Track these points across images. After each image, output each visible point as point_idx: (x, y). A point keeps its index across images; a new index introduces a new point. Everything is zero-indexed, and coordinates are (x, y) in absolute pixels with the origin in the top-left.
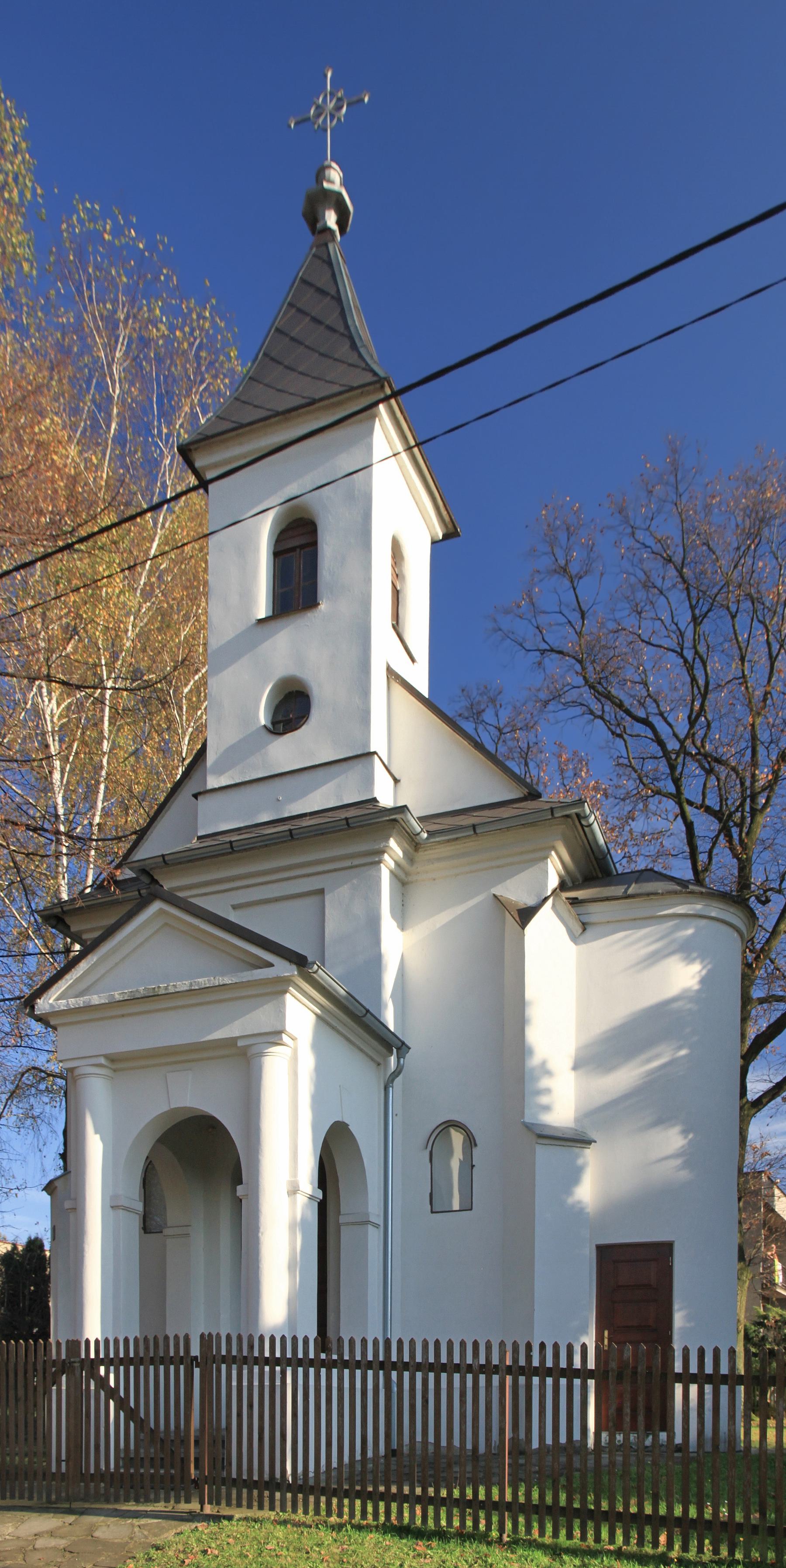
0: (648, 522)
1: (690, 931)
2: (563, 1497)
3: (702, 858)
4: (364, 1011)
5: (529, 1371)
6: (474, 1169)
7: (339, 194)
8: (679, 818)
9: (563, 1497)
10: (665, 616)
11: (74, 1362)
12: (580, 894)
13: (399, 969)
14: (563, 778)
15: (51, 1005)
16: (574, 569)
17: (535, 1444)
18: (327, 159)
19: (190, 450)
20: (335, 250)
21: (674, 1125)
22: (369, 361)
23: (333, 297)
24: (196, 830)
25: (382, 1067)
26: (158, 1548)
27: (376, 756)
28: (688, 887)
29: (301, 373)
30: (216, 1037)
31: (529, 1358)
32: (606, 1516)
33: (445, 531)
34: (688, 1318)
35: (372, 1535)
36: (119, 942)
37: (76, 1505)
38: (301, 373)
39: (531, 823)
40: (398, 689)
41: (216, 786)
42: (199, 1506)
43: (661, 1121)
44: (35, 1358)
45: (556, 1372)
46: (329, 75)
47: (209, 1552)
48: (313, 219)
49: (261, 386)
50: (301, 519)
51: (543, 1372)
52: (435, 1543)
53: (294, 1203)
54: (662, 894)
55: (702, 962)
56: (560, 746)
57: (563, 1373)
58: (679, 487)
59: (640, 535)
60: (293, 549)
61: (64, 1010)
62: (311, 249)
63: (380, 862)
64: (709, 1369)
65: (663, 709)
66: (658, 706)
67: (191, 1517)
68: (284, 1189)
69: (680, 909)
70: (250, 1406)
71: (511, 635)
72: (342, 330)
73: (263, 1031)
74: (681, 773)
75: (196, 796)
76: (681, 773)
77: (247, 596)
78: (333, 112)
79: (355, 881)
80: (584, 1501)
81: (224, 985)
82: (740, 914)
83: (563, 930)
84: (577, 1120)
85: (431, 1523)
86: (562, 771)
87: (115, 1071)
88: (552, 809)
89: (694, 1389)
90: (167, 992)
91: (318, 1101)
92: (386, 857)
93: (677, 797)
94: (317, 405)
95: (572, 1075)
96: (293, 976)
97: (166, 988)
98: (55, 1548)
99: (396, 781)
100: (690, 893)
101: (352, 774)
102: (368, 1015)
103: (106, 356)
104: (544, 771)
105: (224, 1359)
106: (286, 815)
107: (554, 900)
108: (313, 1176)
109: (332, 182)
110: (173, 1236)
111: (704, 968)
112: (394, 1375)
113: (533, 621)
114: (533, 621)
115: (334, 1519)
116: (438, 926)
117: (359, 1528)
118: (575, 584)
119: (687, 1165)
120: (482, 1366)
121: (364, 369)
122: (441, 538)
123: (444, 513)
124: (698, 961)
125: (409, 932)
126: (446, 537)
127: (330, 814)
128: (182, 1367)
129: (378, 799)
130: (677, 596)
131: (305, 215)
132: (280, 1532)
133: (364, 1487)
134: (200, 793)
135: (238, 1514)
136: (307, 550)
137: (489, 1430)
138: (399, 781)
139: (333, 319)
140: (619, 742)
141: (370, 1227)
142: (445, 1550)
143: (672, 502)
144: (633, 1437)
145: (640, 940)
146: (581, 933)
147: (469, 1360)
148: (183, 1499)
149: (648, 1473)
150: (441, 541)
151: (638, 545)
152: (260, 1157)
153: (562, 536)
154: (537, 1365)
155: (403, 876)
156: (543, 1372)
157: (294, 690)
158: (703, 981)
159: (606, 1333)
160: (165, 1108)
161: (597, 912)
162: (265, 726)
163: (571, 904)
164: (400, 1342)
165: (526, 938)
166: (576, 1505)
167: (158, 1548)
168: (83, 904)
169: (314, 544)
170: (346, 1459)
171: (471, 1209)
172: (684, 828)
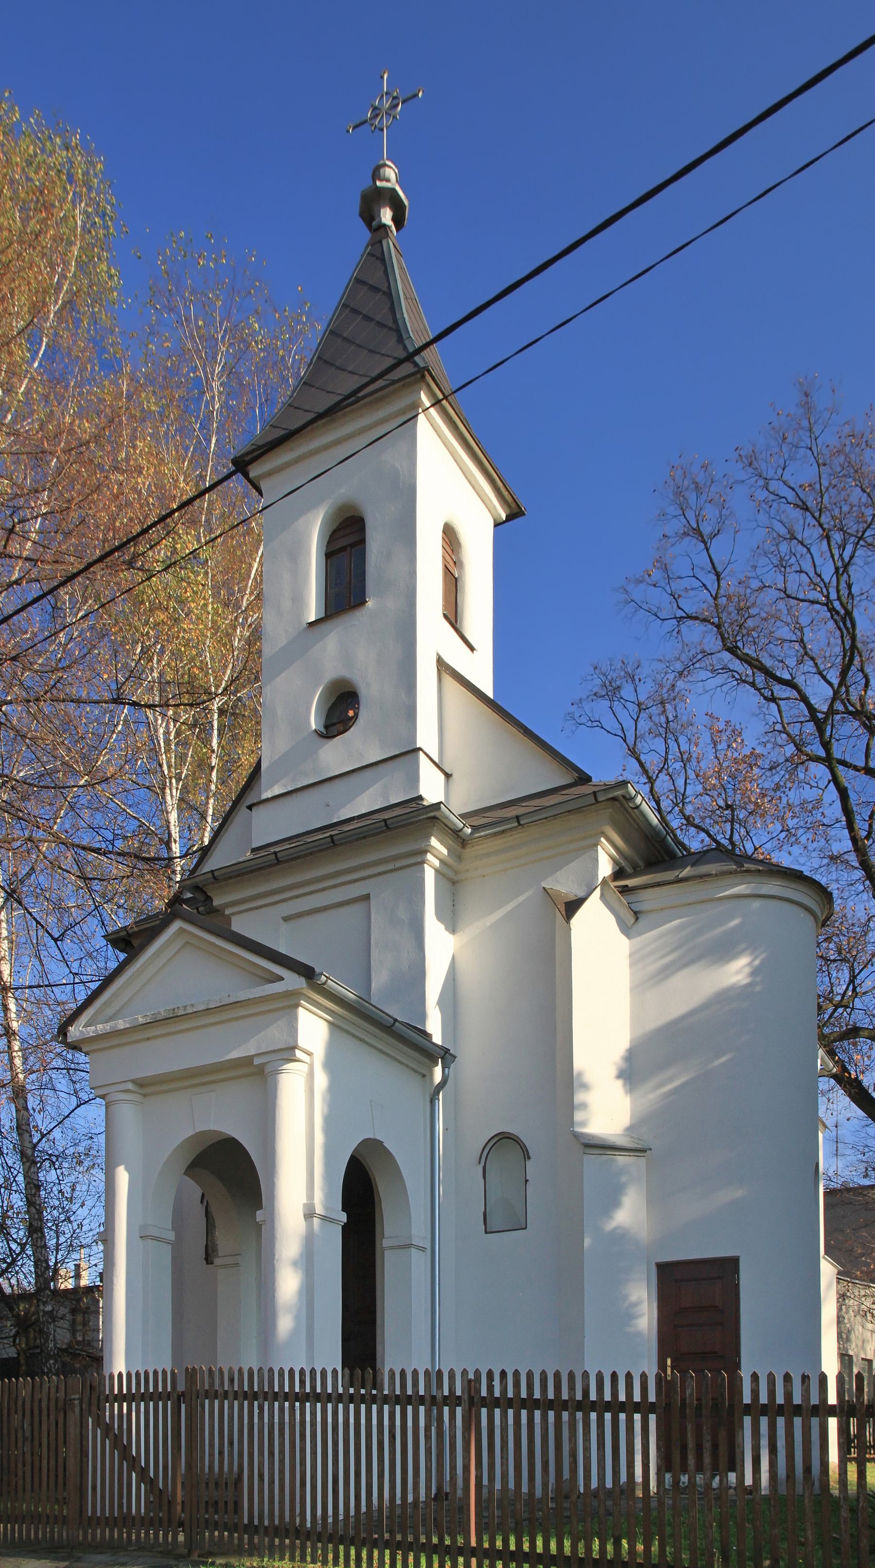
4: (392, 1021)
7: (394, 190)
10: (807, 566)
11: (74, 1399)
12: (630, 882)
16: (706, 530)
20: (390, 245)
23: (384, 293)
27: (421, 752)
33: (508, 512)
36: (143, 964)
40: (449, 681)
48: (369, 216)
50: (353, 517)
57: (523, 1404)
58: (814, 430)
59: (774, 486)
61: (93, 1036)
63: (423, 862)
64: (764, 1399)
70: (231, 1443)
71: (645, 606)
77: (298, 600)
82: (811, 893)
83: (611, 919)
86: (715, 744)
87: (145, 1096)
88: (595, 793)
92: (429, 856)
93: (829, 761)
94: (362, 402)
99: (448, 776)
102: (397, 1023)
105: (207, 1395)
107: (602, 890)
109: (388, 180)
110: (225, 1266)
113: (668, 588)
114: (668, 588)
116: (488, 924)
118: (708, 545)
122: (504, 519)
123: (506, 493)
126: (510, 518)
127: (375, 816)
128: (169, 1403)
129: (424, 796)
131: (362, 215)
138: (451, 775)
140: (773, 706)
143: (807, 448)
144: (699, 1479)
150: (504, 522)
151: (772, 497)
152: (276, 1180)
153: (692, 497)
160: (190, 1133)
161: (649, 899)
162: (315, 730)
163: (620, 892)
169: (362, 541)
171: (526, 1228)
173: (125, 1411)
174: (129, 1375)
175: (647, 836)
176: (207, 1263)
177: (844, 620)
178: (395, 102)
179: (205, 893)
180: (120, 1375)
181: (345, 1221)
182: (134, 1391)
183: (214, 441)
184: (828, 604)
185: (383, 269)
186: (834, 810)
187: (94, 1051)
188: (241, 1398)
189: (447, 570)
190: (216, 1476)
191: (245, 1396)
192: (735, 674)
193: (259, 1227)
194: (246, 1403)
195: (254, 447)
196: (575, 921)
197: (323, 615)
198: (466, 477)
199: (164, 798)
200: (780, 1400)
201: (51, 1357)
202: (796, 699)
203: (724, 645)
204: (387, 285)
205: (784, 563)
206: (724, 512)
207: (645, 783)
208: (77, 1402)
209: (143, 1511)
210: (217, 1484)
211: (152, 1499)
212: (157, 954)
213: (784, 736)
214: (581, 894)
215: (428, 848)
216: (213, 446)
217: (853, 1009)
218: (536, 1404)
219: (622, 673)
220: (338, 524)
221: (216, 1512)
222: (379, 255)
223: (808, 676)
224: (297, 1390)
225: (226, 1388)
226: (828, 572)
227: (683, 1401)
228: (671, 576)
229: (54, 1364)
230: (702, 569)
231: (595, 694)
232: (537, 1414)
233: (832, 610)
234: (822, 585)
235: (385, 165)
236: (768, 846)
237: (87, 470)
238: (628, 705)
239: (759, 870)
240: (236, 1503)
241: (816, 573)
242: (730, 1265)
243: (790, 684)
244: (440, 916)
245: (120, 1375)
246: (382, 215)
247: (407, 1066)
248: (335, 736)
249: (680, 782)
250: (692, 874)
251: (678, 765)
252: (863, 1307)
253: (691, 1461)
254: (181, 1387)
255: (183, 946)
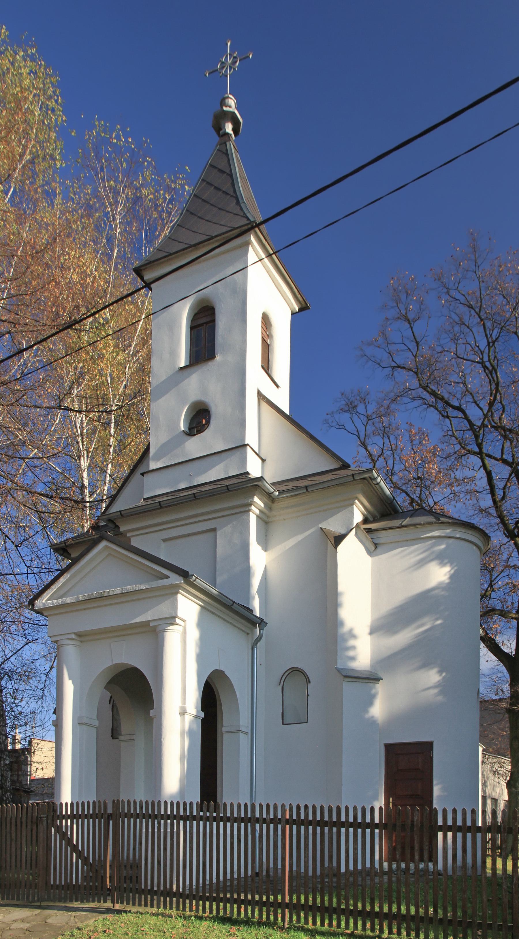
0: (456, 285)
1: (443, 547)
2: (431, 910)
3: (499, 494)
4: (232, 603)
5: (339, 824)
6: (309, 697)
7: (234, 113)
8: (482, 468)
9: (431, 910)
11: (43, 817)
13: (263, 575)
14: (412, 445)
15: (44, 604)
16: (411, 316)
17: (343, 870)
18: (227, 93)
19: (141, 270)
20: (231, 146)
21: (433, 668)
22: (246, 212)
23: (228, 174)
24: (142, 494)
25: (250, 635)
26: (79, 929)
28: (439, 520)
29: (207, 221)
30: (138, 621)
31: (298, 814)
32: (343, 911)
33: (300, 307)
34: (444, 789)
35: (206, 922)
37: (44, 904)
38: (207, 221)
39: (342, 484)
40: (264, 405)
41: (155, 468)
42: (112, 904)
43: (426, 665)
44: (22, 814)
45: (355, 825)
46: (229, 44)
47: (107, 932)
48: (218, 128)
49: (184, 229)
50: (207, 306)
51: (348, 825)
52: (242, 928)
53: (183, 720)
54: (424, 524)
55: (451, 565)
56: (410, 425)
57: (318, 823)
58: (478, 261)
60: (201, 325)
62: (217, 146)
63: (249, 511)
64: (459, 823)
65: (476, 399)
66: (473, 397)
67: (108, 911)
68: (177, 712)
69: (436, 533)
70: (141, 843)
71: (373, 359)
72: (232, 193)
73: (164, 617)
74: (482, 440)
75: (143, 474)
76: (482, 440)
77: (174, 354)
78: (231, 65)
79: (234, 523)
80: (347, 905)
81: (141, 590)
83: (363, 548)
84: (372, 666)
85: (242, 915)
86: (412, 441)
87: (82, 642)
88: (353, 475)
89: (450, 834)
90: (109, 594)
91: (201, 658)
92: (253, 507)
93: (480, 454)
95: (369, 638)
96: (181, 583)
97: (108, 592)
98: (22, 929)
99: (263, 460)
100: (441, 523)
101: (235, 457)
103: (112, 210)
104: (400, 441)
105: (126, 815)
106: (195, 484)
107: (356, 530)
108: (197, 703)
109: (230, 107)
111: (452, 569)
112: (257, 825)
113: (387, 349)
114: (387, 349)
115: (188, 913)
116: (287, 548)
117: (200, 918)
118: (412, 325)
119: (441, 693)
120: (272, 819)
121: (242, 216)
123: (299, 296)
124: (448, 565)
125: (269, 552)
126: (301, 310)
127: (220, 483)
128: (102, 820)
129: (250, 472)
130: (478, 330)
132: (153, 920)
133: (218, 895)
134: (145, 473)
135: (134, 909)
136: (209, 325)
137: (275, 859)
139: (226, 187)
140: (447, 420)
141: (241, 735)
142: (247, 931)
143: (473, 271)
145: (411, 553)
146: (374, 550)
147: (264, 816)
148: (102, 901)
149: (394, 886)
150: (297, 312)
152: (163, 693)
153: (403, 297)
154: (303, 818)
155: (265, 518)
156: (348, 825)
157: (202, 408)
158: (452, 577)
159: (391, 800)
160: (111, 664)
161: (384, 537)
162: (183, 431)
163: (367, 532)
164: (261, 806)
165: (338, 554)
166: (343, 907)
167: (79, 929)
168: (73, 542)
169: (213, 321)
170: (221, 878)
171: (307, 722)
172: (485, 475)
173: (69, 824)
174: (72, 804)
175: (382, 500)
176: (113, 738)
177: (491, 373)
178: (235, 60)
179: (115, 523)
180: (66, 804)
181: (203, 717)
182: (80, 813)
183: (116, 252)
184: (482, 363)
185: (227, 159)
186: (482, 483)
187: (50, 615)
188: (147, 817)
189: (264, 341)
190: (131, 862)
191: (150, 816)
192: (425, 401)
193: (152, 719)
194: (97, 820)
195: (147, 262)
196: (339, 548)
197: (188, 364)
198: (276, 286)
199: (80, 462)
200: (469, 823)
201: (8, 791)
202: (462, 418)
203: (420, 385)
204: (229, 169)
205: (456, 338)
206: (422, 306)
207: (370, 463)
208: (44, 819)
209: (80, 881)
210: (131, 867)
211: (91, 875)
212: (91, 560)
213: (453, 438)
214: (343, 532)
215: (252, 503)
216: (115, 255)
217: (490, 598)
218: (326, 824)
219: (358, 398)
220: (198, 310)
221: (131, 882)
222: (225, 151)
223: (469, 404)
224: (182, 813)
225: (138, 812)
226: (483, 344)
227: (412, 821)
228: (389, 342)
229: (10, 796)
230: (408, 339)
231: (341, 410)
232: (302, 828)
233: (485, 367)
234: (479, 352)
235: (228, 97)
236: (442, 502)
237: (41, 268)
238: (361, 416)
239: (449, 523)
240: (137, 877)
241: (476, 345)
242: (430, 745)
243: (459, 409)
244: (259, 542)
245: (66, 804)
246: (226, 127)
247: (239, 628)
248: (195, 435)
249: (390, 462)
250: (409, 523)
251: (389, 453)
252: (494, 769)
253: (417, 857)
254: (110, 811)
255: (107, 557)
